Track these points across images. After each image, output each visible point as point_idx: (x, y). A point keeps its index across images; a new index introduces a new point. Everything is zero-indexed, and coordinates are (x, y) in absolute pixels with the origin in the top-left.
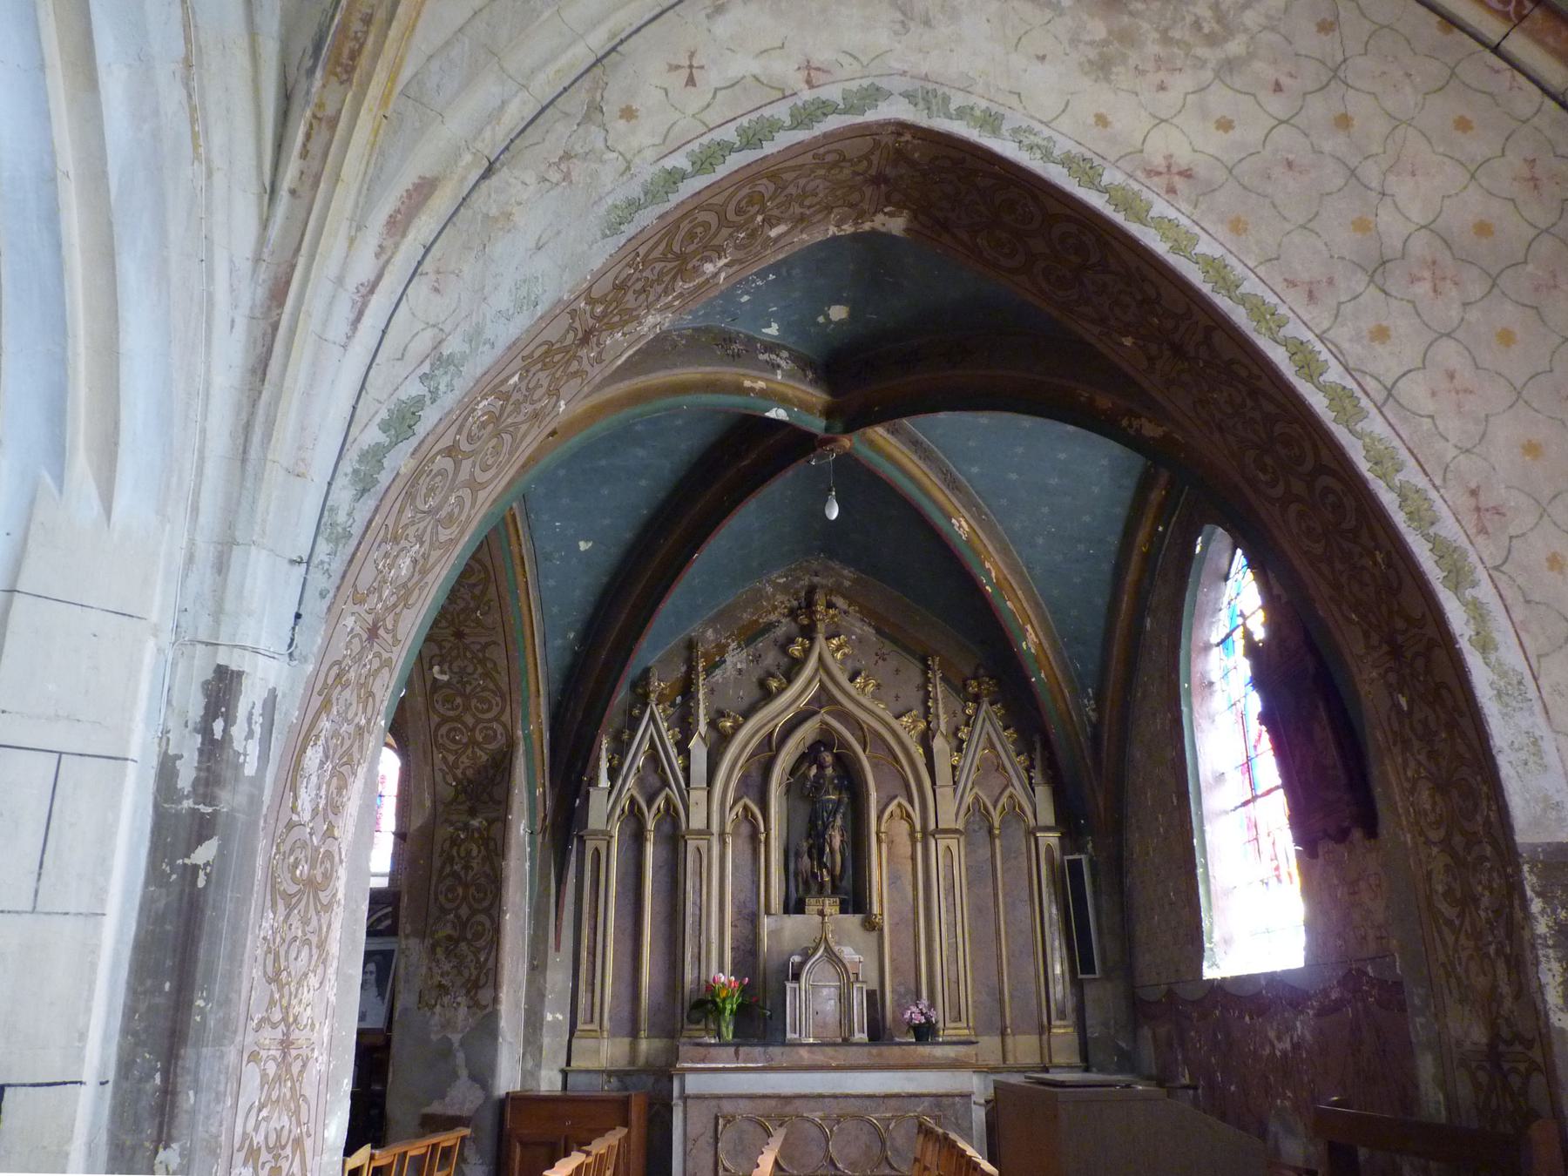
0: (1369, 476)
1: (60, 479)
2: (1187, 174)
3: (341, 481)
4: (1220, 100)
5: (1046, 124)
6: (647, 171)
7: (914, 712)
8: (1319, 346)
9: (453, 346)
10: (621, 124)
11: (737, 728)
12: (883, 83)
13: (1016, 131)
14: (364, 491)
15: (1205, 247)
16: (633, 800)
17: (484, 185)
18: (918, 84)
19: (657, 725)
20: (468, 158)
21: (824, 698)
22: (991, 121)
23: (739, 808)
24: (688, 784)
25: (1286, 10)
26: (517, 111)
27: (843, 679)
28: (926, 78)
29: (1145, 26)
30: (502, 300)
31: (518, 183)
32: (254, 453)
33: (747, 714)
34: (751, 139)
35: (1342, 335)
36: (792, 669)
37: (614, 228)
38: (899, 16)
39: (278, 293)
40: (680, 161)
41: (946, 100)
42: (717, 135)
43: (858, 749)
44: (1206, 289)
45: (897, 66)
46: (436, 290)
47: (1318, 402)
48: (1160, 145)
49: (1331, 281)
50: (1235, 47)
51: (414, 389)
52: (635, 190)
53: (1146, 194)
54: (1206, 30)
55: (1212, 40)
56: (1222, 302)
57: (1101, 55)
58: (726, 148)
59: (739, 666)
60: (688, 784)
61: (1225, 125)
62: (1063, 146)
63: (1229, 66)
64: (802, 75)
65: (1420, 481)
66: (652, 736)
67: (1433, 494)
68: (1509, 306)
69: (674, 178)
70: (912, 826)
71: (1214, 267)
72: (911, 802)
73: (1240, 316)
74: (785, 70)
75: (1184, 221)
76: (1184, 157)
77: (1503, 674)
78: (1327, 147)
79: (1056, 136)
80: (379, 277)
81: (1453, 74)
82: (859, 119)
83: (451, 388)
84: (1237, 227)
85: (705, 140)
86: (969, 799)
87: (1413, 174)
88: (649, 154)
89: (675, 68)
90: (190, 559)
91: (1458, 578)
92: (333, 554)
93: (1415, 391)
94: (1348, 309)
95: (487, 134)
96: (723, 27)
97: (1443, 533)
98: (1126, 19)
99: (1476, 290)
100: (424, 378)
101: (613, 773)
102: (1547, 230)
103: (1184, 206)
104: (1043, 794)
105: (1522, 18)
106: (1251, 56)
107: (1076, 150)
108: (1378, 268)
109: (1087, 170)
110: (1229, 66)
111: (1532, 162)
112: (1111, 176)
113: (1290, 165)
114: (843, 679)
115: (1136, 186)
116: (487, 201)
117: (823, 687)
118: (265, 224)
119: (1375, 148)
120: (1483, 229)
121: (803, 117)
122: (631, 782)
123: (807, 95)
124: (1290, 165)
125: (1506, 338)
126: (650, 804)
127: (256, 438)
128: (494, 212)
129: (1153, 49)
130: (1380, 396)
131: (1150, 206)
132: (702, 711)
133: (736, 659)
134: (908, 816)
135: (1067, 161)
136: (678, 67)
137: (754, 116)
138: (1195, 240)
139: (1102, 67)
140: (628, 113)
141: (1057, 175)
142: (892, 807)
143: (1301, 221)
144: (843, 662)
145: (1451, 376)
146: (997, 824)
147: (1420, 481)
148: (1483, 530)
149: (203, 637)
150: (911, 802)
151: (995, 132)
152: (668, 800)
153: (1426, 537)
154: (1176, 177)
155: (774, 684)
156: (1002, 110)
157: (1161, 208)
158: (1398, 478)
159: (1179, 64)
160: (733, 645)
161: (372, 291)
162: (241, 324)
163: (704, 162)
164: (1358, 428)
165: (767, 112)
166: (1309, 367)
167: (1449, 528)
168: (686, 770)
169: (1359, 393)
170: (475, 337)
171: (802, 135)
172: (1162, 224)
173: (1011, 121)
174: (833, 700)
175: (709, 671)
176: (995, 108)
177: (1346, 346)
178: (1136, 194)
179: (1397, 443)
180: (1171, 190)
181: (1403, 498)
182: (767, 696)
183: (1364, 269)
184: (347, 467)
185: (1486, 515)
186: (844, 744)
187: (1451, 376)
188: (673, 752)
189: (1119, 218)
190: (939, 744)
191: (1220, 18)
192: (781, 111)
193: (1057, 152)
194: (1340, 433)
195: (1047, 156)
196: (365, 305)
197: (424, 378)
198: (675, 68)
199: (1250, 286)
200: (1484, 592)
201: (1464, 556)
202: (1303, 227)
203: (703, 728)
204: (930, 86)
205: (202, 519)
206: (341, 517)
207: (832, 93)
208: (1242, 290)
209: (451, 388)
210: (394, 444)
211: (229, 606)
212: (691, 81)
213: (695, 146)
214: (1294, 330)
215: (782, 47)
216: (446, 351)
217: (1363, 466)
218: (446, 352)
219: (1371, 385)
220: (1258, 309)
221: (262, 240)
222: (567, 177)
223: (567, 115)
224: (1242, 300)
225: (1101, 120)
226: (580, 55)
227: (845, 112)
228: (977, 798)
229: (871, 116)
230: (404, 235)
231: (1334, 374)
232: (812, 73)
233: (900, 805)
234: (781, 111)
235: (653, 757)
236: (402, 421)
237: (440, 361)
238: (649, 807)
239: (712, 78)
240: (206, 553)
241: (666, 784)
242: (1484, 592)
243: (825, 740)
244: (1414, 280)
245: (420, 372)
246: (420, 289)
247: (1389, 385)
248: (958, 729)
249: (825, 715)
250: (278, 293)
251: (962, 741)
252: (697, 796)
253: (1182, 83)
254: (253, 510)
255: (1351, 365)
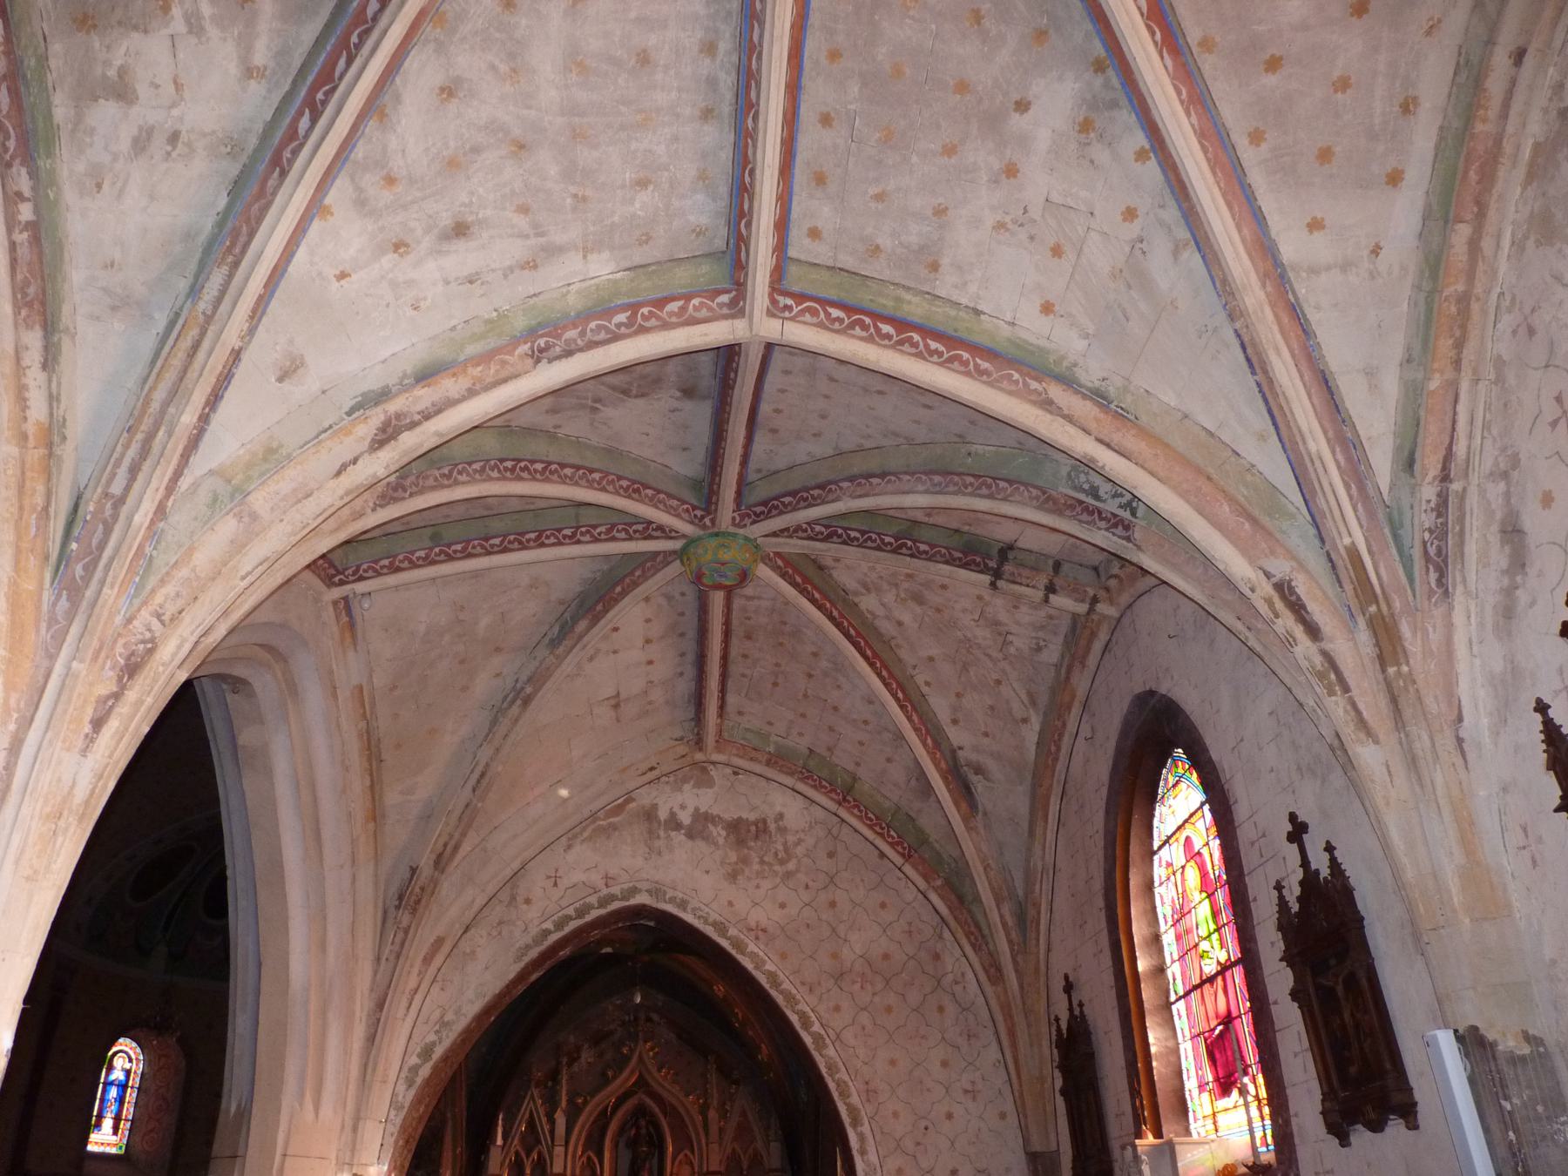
0: (825, 1075)
1: (301, 1105)
2: (764, 930)
3: (401, 1081)
4: (783, 894)
5: (707, 906)
6: (534, 931)
7: (698, 1092)
8: (812, 1014)
9: (449, 1017)
10: (525, 907)
11: (585, 1103)
12: (639, 885)
13: (694, 909)
14: (410, 1086)
15: (770, 967)
16: (517, 1153)
17: (465, 936)
18: (654, 885)
19: (533, 1103)
20: (457, 926)
21: (642, 1083)
22: (683, 905)
23: (584, 1159)
24: (553, 1141)
25: (815, 847)
26: (480, 901)
27: (654, 1070)
28: (657, 882)
29: (753, 854)
30: (470, 994)
31: (479, 936)
32: (368, 1078)
33: (593, 1094)
34: (580, 913)
35: (821, 1009)
36: (621, 1063)
37: (518, 959)
38: (647, 850)
39: (380, 1005)
40: (549, 925)
41: (665, 893)
42: (564, 912)
43: (660, 1116)
44: (767, 986)
45: (645, 876)
46: (442, 989)
47: (808, 1040)
48: (757, 916)
49: (819, 984)
50: (791, 866)
51: (432, 1037)
52: (528, 939)
53: (747, 940)
54: (780, 857)
55: (782, 862)
56: (773, 993)
57: (733, 870)
58: (568, 918)
59: (589, 1060)
60: (553, 1141)
61: (783, 906)
62: (714, 916)
63: (788, 875)
64: (604, 881)
65: (846, 1078)
66: (531, 1111)
67: (850, 1084)
68: (892, 994)
69: (546, 933)
70: (693, 1169)
71: (772, 976)
72: (693, 1153)
73: (780, 999)
74: (596, 878)
75: (761, 954)
76: (764, 923)
77: (869, 1165)
78: (824, 917)
79: (710, 911)
80: (419, 986)
81: (882, 880)
82: (627, 903)
83: (447, 1037)
84: (783, 956)
85: (560, 914)
86: (729, 1150)
87: (859, 930)
88: (536, 922)
89: (549, 877)
90: (343, 1127)
91: (856, 1122)
92: (396, 1116)
93: (848, 1036)
94: (825, 996)
95: (467, 913)
96: (571, 856)
97: (852, 1102)
98: (746, 851)
99: (879, 986)
100: (437, 1032)
101: (505, 1138)
102: (912, 957)
103: (762, 947)
104: (775, 1147)
105: (910, 856)
106: (797, 871)
107: (719, 918)
108: (839, 977)
109: (721, 928)
110: (788, 875)
111: (910, 924)
112: (732, 932)
113: (808, 925)
114: (654, 1070)
115: (742, 937)
116: (465, 946)
117: (641, 1075)
118: (375, 973)
119: (845, 918)
120: (886, 956)
121: (603, 902)
122: (516, 1142)
123: (605, 891)
124: (808, 925)
125: (889, 1009)
126: (528, 1155)
127: (369, 1071)
128: (468, 951)
129: (756, 867)
130: (833, 1038)
131: (747, 946)
132: (564, 1093)
133: (587, 1056)
134: (691, 1163)
135: (715, 924)
136: (550, 877)
137: (581, 902)
138: (764, 963)
139: (733, 876)
140: (528, 901)
141: (709, 931)
142: (681, 1157)
143: (810, 953)
144: (653, 1058)
145: (864, 1028)
146: (745, 1167)
147: (846, 1078)
148: (868, 1101)
149: (347, 1161)
150: (693, 1153)
151: (685, 910)
152: (540, 1154)
153: (845, 1103)
154: (759, 932)
155: (610, 1073)
156: (688, 898)
157: (752, 947)
158: (837, 1076)
159: (766, 875)
160: (586, 1046)
161: (415, 993)
162: (364, 1019)
163: (559, 925)
164: (823, 1053)
165: (587, 900)
166: (806, 1024)
167: (855, 1099)
168: (552, 1132)
169: (825, 1036)
170: (458, 1012)
171: (602, 912)
172: (753, 956)
173: (694, 903)
174: (647, 1084)
175: (569, 1065)
176: (685, 897)
177: (822, 1014)
178: (742, 941)
179: (838, 1060)
180: (757, 938)
181: (838, 1085)
182: (605, 1081)
183: (833, 977)
184: (403, 1075)
185: (870, 1093)
186: (653, 1115)
187: (864, 1028)
188: (544, 1120)
189: (733, 952)
190: (712, 1114)
191: (786, 850)
192: (593, 900)
193: (711, 920)
194: (815, 1054)
195: (706, 922)
196: (412, 999)
197: (437, 1032)
198: (549, 877)
199: (786, 985)
200: (866, 1129)
201: (859, 1112)
202: (811, 957)
203: (564, 1104)
204: (658, 886)
205: (348, 1109)
206: (400, 1098)
207: (616, 890)
208: (783, 987)
209: (447, 1037)
210: (423, 1064)
211: (358, 1147)
212: (555, 884)
213: (555, 917)
214: (802, 1006)
215: (596, 867)
216: (446, 1019)
217: (824, 1071)
218: (446, 1020)
219: (831, 1032)
220: (789, 997)
221: (374, 981)
222: (500, 933)
223: (501, 901)
224: (781, 992)
225: (730, 904)
226: (508, 872)
227: (622, 900)
228: (734, 1150)
229: (632, 902)
230: (430, 965)
231: (816, 1027)
232: (608, 880)
233: (686, 1155)
234: (593, 900)
235: (531, 1125)
236: (426, 1052)
237: (445, 1024)
238: (527, 1158)
239: (564, 883)
240: (349, 1123)
241: (539, 1142)
242: (866, 1129)
243: (641, 1111)
244: (854, 982)
245: (435, 1029)
246: (435, 989)
247: (838, 1031)
248: (724, 1104)
249: (643, 1096)
250: (380, 1005)
251: (727, 1111)
252: (559, 1150)
253: (766, 884)
254: (368, 1102)
255: (824, 1022)
